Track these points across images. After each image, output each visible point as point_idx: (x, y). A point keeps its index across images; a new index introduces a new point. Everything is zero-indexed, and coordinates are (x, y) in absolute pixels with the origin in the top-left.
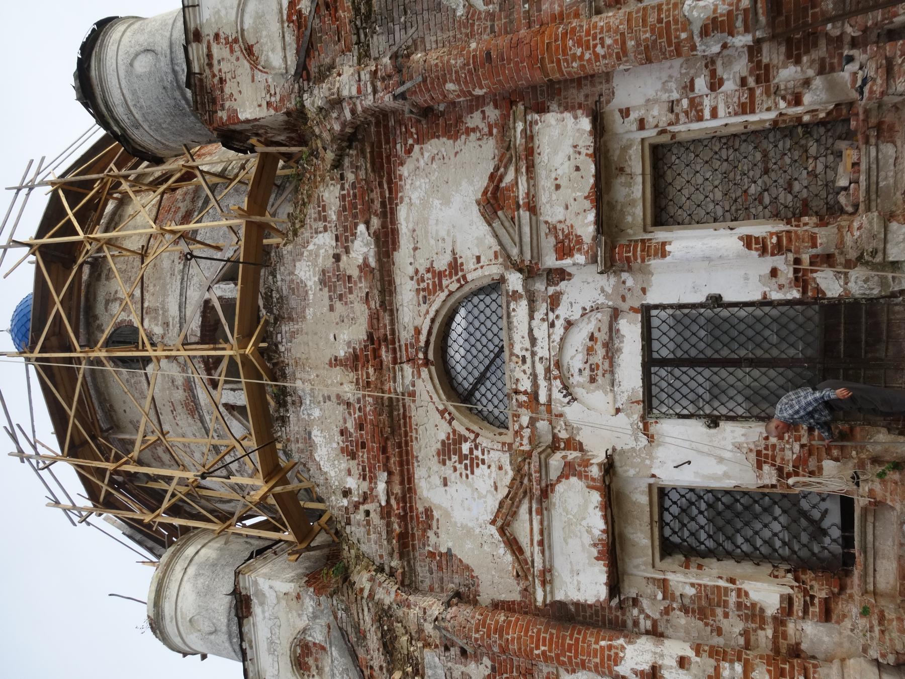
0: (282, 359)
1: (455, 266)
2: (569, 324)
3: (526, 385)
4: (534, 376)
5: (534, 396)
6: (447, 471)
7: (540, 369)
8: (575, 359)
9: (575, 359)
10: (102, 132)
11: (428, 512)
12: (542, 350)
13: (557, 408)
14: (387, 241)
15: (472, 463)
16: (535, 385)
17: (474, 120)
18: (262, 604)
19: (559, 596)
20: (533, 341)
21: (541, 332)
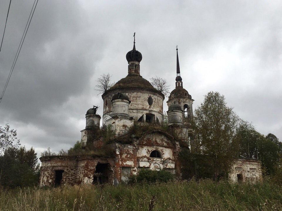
0: (116, 108)
1: (163, 154)
2: (159, 165)
3: (154, 160)
4: (155, 161)
5: (154, 161)
6: (147, 150)
7: (156, 161)
8: (156, 165)
9: (156, 165)
10: (96, 114)
11: (143, 147)
12: (157, 162)
13: (153, 163)
14: (166, 147)
15: (147, 153)
16: (154, 161)
17: (173, 157)
18: (107, 80)
19: (129, 127)
20: (158, 161)
21: (159, 162)
